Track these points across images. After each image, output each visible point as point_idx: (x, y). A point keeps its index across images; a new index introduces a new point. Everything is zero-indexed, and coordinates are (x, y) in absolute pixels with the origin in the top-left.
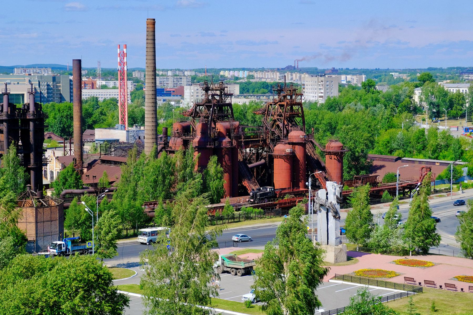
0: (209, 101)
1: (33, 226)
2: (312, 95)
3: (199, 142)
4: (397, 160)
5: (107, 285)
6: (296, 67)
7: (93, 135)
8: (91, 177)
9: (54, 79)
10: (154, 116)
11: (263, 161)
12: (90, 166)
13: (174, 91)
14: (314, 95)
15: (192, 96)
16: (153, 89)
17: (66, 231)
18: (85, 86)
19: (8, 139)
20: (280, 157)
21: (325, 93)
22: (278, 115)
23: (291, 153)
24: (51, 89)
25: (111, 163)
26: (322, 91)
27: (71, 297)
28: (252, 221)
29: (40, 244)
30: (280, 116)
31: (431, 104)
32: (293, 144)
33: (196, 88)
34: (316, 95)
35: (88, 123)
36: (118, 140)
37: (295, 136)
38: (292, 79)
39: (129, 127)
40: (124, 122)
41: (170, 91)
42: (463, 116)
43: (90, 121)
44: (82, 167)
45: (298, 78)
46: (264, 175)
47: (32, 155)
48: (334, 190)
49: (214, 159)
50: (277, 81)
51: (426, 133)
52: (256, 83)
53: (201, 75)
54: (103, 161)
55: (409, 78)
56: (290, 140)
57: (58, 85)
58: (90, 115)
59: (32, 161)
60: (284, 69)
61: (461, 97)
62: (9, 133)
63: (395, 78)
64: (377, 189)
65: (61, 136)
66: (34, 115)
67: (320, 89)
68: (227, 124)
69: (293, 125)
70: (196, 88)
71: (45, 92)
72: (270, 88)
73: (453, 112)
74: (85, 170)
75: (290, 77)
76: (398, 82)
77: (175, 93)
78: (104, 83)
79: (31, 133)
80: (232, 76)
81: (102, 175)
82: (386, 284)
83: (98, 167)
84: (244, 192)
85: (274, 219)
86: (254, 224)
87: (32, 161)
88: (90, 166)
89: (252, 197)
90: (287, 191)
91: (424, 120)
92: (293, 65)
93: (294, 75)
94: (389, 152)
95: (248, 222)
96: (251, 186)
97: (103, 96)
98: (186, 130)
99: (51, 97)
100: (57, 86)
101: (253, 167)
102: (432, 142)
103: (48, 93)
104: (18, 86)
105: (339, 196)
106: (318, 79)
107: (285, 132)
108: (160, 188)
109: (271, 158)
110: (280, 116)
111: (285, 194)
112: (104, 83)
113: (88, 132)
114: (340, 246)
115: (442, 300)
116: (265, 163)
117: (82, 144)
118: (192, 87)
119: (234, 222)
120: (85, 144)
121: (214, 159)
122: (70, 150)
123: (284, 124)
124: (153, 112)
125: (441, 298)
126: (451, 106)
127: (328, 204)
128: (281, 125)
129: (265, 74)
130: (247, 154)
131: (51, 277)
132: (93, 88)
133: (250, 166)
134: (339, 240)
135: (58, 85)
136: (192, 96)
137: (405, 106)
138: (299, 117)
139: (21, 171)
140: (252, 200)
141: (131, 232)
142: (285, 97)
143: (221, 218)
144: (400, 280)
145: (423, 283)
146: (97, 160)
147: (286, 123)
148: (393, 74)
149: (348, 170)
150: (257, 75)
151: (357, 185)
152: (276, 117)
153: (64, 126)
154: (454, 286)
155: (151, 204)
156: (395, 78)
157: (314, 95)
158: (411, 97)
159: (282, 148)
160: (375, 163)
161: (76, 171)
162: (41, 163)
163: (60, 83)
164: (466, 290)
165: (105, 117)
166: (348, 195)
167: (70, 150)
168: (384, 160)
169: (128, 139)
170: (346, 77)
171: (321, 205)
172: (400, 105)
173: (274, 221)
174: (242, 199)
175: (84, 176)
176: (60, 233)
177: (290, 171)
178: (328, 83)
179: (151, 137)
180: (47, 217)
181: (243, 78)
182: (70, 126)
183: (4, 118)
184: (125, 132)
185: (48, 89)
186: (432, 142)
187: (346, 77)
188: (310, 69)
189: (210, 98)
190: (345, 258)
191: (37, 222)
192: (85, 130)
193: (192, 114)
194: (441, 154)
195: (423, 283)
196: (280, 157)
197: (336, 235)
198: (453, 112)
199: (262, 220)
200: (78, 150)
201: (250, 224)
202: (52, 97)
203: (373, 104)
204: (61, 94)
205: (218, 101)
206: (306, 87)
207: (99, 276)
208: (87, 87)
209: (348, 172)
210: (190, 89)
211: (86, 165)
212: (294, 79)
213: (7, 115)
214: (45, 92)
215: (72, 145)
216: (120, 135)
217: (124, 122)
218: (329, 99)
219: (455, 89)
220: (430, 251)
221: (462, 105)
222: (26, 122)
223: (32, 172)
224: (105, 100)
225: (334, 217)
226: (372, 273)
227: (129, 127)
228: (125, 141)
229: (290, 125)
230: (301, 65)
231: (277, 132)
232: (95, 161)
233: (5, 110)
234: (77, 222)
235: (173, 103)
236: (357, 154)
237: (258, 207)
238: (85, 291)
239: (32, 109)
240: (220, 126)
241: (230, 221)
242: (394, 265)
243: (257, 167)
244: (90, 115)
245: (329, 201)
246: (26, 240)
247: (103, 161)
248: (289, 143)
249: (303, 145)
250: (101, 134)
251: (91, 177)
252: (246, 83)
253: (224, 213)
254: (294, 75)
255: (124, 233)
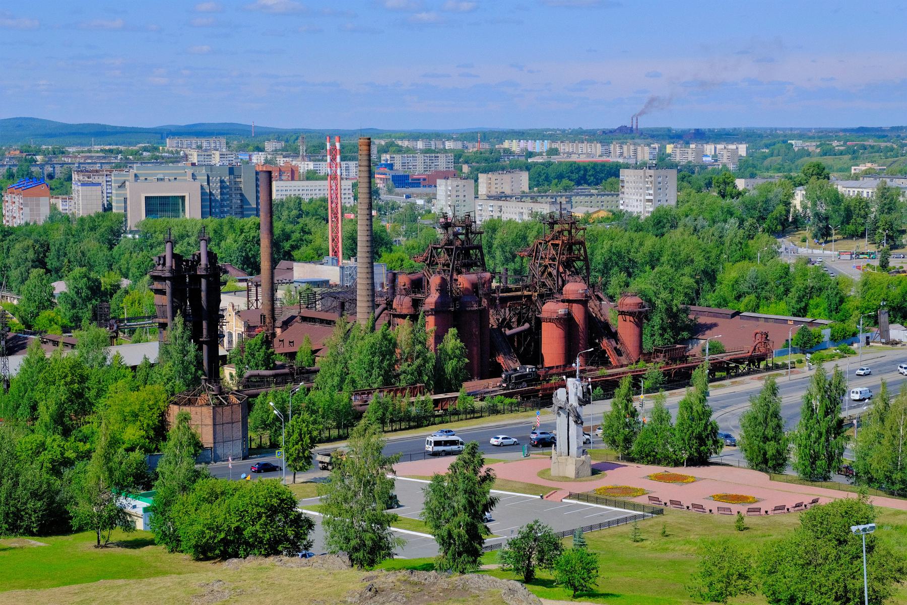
0: (450, 242)
1: (210, 429)
2: (635, 197)
3: (436, 303)
4: (733, 316)
5: (291, 509)
6: (634, 127)
7: (291, 269)
8: (286, 343)
9: (231, 171)
10: (369, 270)
11: (527, 326)
12: (286, 324)
13: (424, 179)
14: (638, 197)
15: (450, 196)
16: (368, 233)
17: (251, 434)
18: (280, 175)
19: (172, 302)
20: (550, 320)
21: (655, 195)
22: (550, 259)
23: (565, 315)
24: (227, 187)
25: (315, 322)
26: (651, 192)
27: (253, 522)
28: (499, 416)
29: (220, 451)
30: (553, 259)
31: (817, 215)
32: (570, 301)
33: (455, 183)
34: (642, 198)
35: (284, 251)
36: (328, 281)
37: (573, 291)
38: (621, 154)
39: (344, 258)
40: (336, 253)
41: (419, 179)
42: (862, 236)
43: (287, 246)
44: (274, 327)
45: (632, 154)
46: (529, 345)
47: (204, 324)
48: (575, 390)
49: (453, 331)
50: (597, 159)
51: (792, 270)
52: (560, 163)
53: (472, 148)
54: (305, 319)
55: (818, 150)
56: (564, 297)
57: (238, 180)
58: (287, 237)
59: (205, 332)
60: (615, 131)
61: (864, 205)
62: (174, 294)
63: (796, 149)
64: (685, 365)
65: (243, 269)
66: (206, 269)
67: (648, 188)
68: (473, 277)
69: (572, 272)
70: (455, 183)
71: (217, 192)
72: (582, 172)
73: (851, 227)
74: (278, 331)
75: (618, 151)
76: (801, 157)
77: (426, 183)
78: (311, 166)
79: (203, 294)
80: (522, 150)
81: (301, 340)
82: (625, 505)
83: (297, 326)
84: (496, 371)
85: (530, 413)
86: (500, 421)
87: (205, 332)
88: (286, 324)
89: (505, 381)
90: (554, 371)
91: (804, 241)
92: (629, 126)
93: (625, 147)
94: (735, 298)
95: (493, 418)
96: (509, 364)
97: (309, 192)
98: (417, 285)
99: (225, 200)
100: (236, 183)
101: (513, 335)
102: (799, 283)
103: (222, 194)
104: (176, 183)
105: (581, 397)
106: (645, 173)
107: (560, 283)
108: (376, 372)
109: (539, 322)
110: (553, 259)
111: (551, 375)
112: (311, 166)
113: (283, 264)
114: (583, 457)
115: (680, 524)
116: (530, 329)
117: (273, 289)
118: (449, 182)
119: (474, 418)
120: (279, 287)
121: (453, 331)
122: (257, 300)
123: (558, 271)
124: (368, 265)
125: (682, 521)
126: (848, 216)
127: (568, 407)
128: (554, 273)
129: (577, 146)
130: (496, 322)
131: (235, 501)
132: (293, 179)
133: (508, 332)
134: (581, 450)
135: (238, 180)
136: (450, 196)
137: (776, 219)
138: (580, 260)
139: (192, 347)
140: (505, 385)
141: (335, 433)
142: (561, 232)
143: (456, 413)
144: (643, 500)
145: (668, 504)
146: (295, 317)
147: (561, 270)
148: (793, 142)
149: (660, 332)
150: (563, 147)
151: (657, 360)
152: (547, 262)
153: (247, 255)
154: (701, 507)
155: (364, 394)
156: (796, 149)
157: (638, 197)
158: (787, 204)
159: (552, 309)
160: (702, 320)
161: (266, 327)
162: (215, 316)
163: (240, 177)
164: (715, 511)
165: (310, 237)
166: (640, 376)
167: (257, 300)
168: (716, 315)
169: (342, 279)
170: (715, 148)
171: (560, 408)
172: (769, 216)
173: (528, 416)
174: (492, 384)
175: (276, 340)
176: (243, 437)
177: (563, 340)
178: (660, 179)
179: (365, 299)
180: (227, 418)
181: (540, 154)
182: (257, 255)
183: (168, 274)
184: (338, 268)
185: (222, 188)
186: (799, 283)
187: (715, 148)
188: (657, 130)
189: (451, 237)
190: (590, 472)
191: (214, 425)
192: (279, 260)
193: (426, 260)
194: (811, 302)
195: (668, 504)
196: (550, 320)
197: (578, 444)
198: (851, 227)
199: (513, 415)
200: (267, 303)
201: (495, 421)
202: (228, 199)
203: (722, 218)
204: (242, 195)
205: (463, 242)
206: (626, 185)
207: (282, 501)
208: (283, 178)
209: (661, 335)
210: (446, 185)
211: (279, 323)
212: (625, 154)
213: (171, 271)
214: (217, 192)
215: (259, 289)
216: (330, 273)
217: (336, 253)
218: (658, 210)
219: (852, 190)
220: (712, 460)
221: (865, 217)
222: (196, 279)
223: (205, 347)
224: (311, 200)
225: (576, 422)
226: (615, 491)
227: (344, 258)
228: (338, 282)
229: (568, 273)
230: (645, 123)
231: (549, 283)
232: (293, 318)
233: (168, 263)
234: (263, 422)
235: (420, 202)
236: (675, 309)
237: (510, 395)
238: (267, 517)
239: (204, 260)
240: (464, 281)
241: (468, 416)
242: (648, 481)
243: (519, 334)
244: (287, 237)
245: (570, 403)
246: (201, 447)
247: (305, 319)
248: (563, 301)
249: (584, 302)
250: (302, 272)
251: (286, 343)
252: (542, 164)
253: (459, 406)
254: (625, 147)
255: (326, 434)
